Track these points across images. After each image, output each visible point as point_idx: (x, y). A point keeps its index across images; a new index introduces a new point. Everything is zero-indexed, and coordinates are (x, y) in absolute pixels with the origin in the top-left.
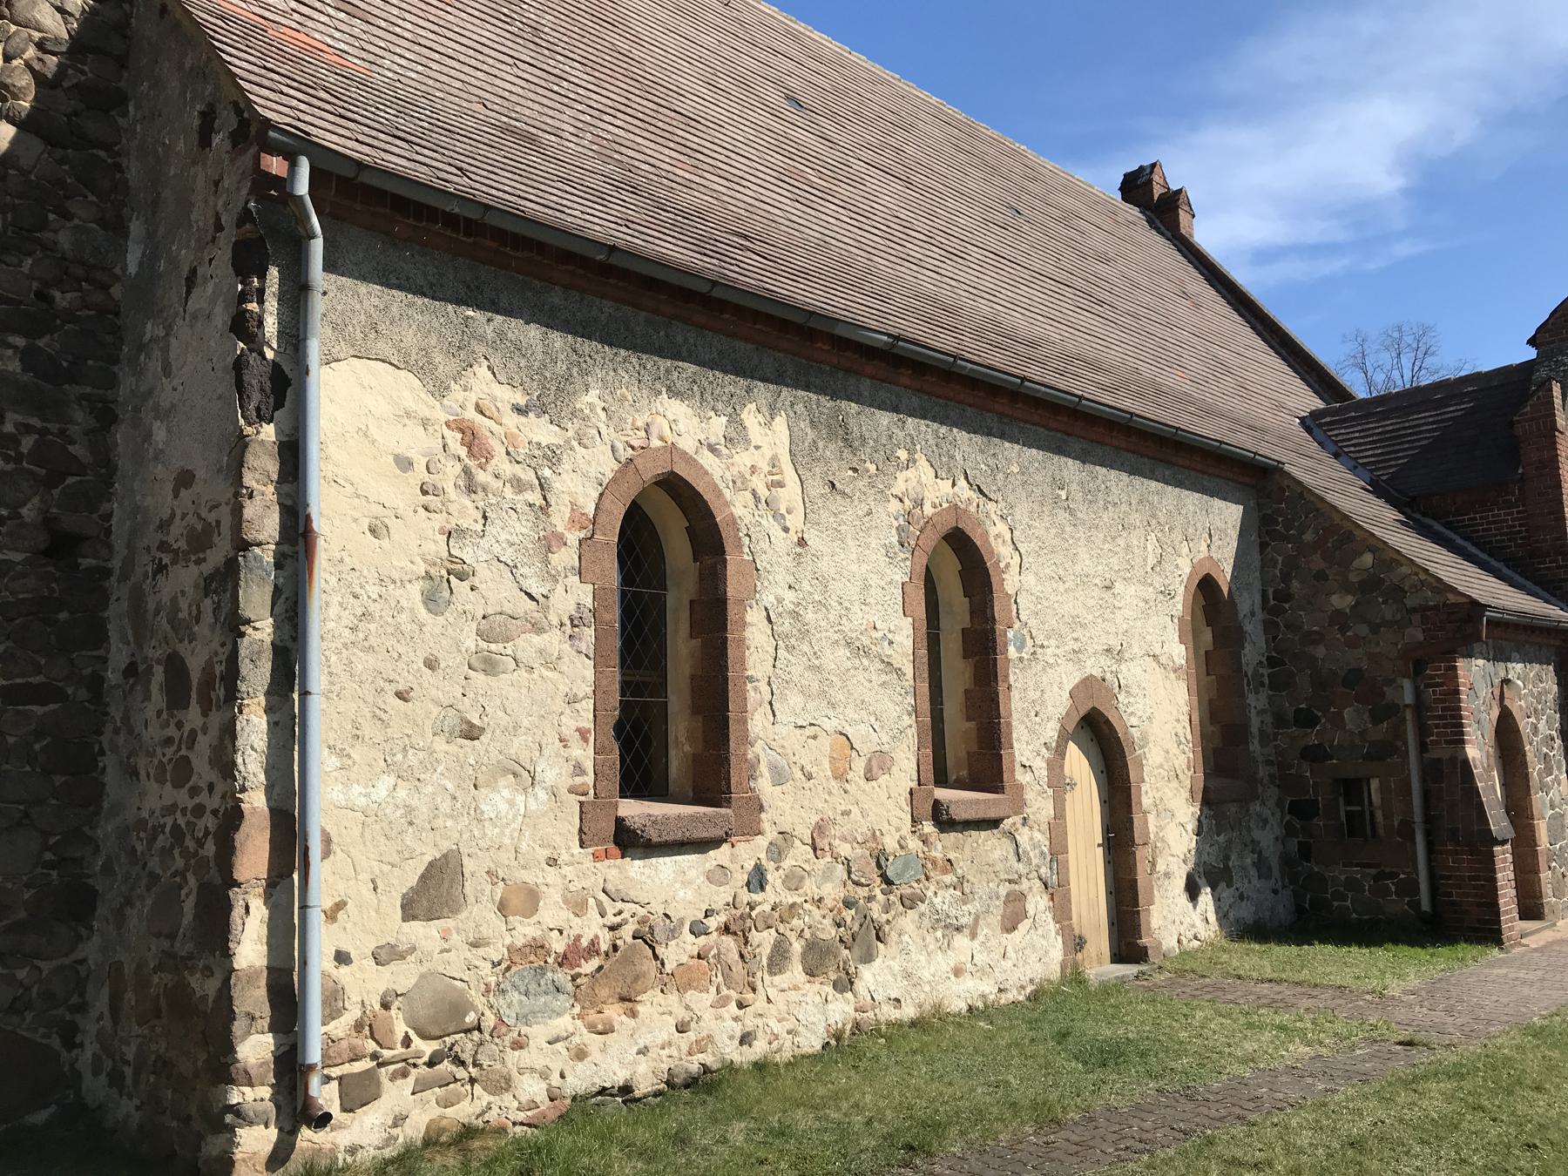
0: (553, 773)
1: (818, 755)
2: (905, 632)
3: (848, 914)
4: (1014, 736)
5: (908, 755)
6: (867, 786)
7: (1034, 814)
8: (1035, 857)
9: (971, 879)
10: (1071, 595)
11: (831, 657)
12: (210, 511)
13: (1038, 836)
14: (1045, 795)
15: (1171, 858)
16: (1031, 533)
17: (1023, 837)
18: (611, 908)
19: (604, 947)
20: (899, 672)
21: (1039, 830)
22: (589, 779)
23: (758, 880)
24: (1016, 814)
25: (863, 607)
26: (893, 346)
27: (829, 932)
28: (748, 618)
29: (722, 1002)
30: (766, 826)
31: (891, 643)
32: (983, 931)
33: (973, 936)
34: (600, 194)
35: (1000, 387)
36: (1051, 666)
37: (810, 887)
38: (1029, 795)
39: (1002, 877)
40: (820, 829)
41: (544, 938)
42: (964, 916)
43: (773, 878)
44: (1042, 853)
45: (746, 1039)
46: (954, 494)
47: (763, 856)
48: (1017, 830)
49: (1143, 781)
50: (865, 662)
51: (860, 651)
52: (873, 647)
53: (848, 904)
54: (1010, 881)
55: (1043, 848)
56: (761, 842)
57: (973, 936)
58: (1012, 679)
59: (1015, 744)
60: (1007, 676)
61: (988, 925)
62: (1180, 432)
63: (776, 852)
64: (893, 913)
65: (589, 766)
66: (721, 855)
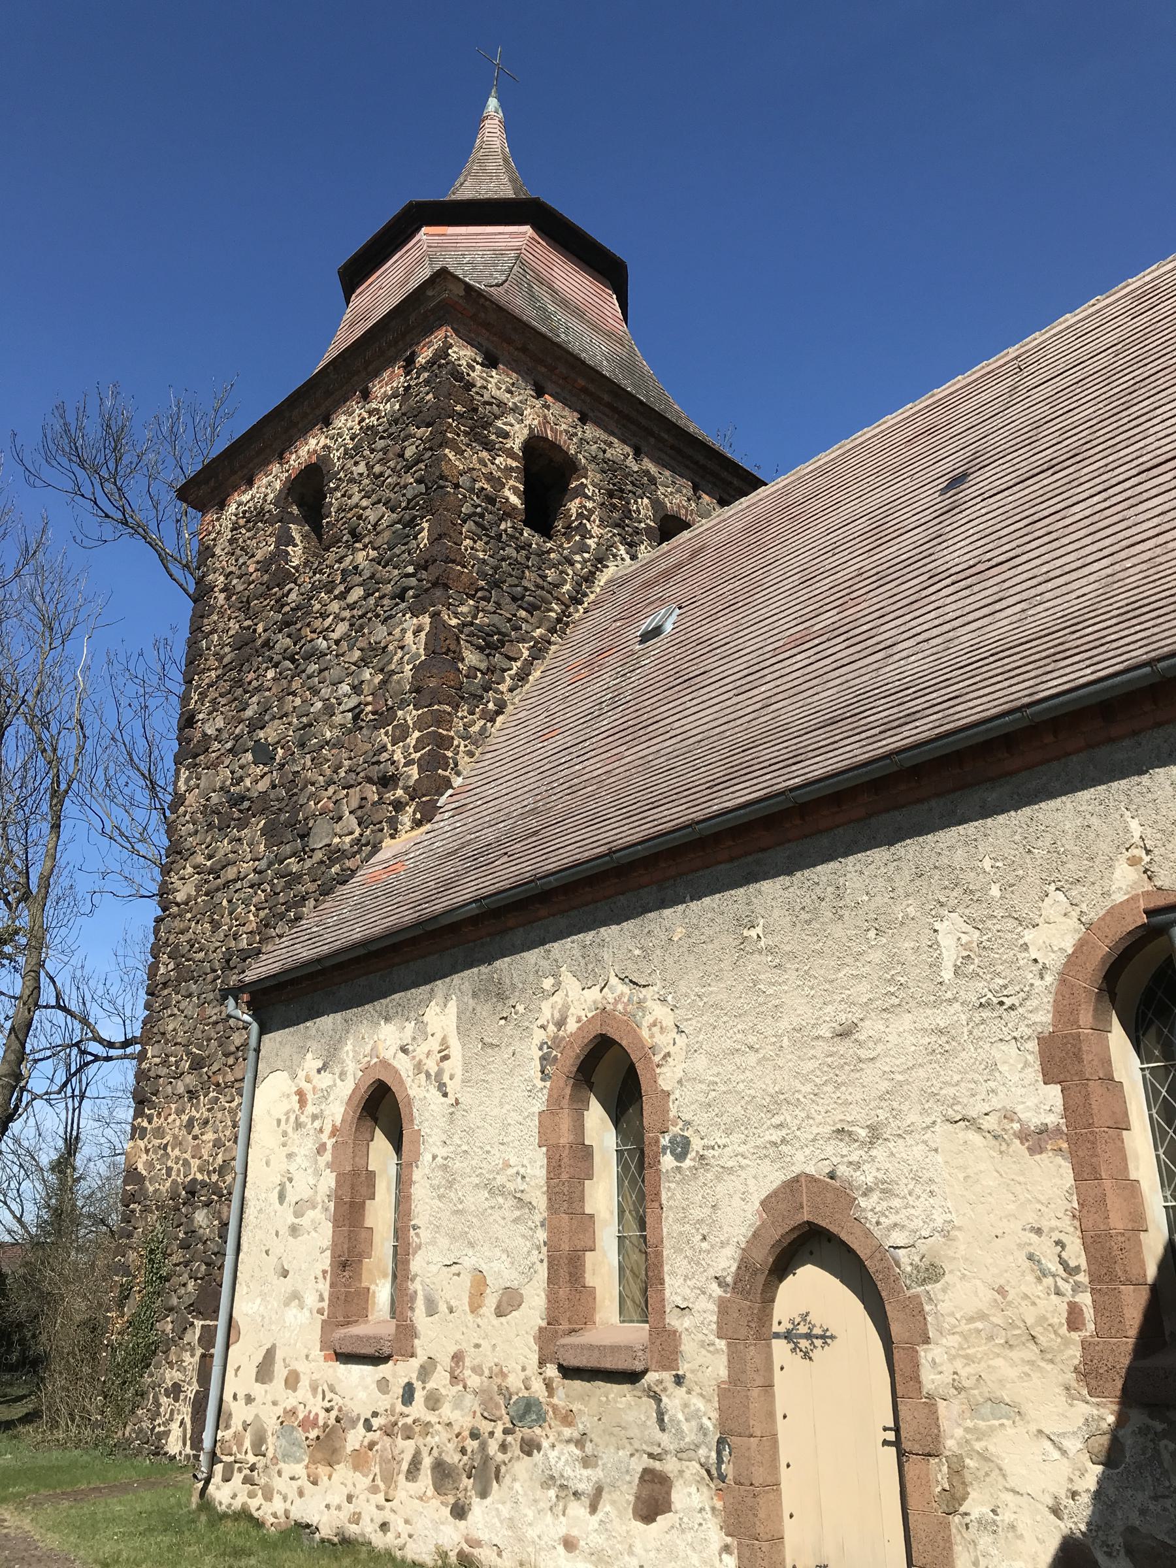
0: (311, 1300)
1: (456, 1292)
2: (539, 1163)
3: (472, 1445)
4: (666, 1268)
5: (538, 1291)
6: (496, 1321)
7: (693, 1371)
8: (691, 1431)
9: (596, 1439)
10: (769, 1065)
11: (472, 1200)
12: (1042, 978)
13: (698, 1403)
14: (711, 1348)
15: (1009, 1497)
16: (701, 1004)
17: (674, 1401)
18: (329, 1395)
19: (321, 1423)
20: (530, 1206)
21: (701, 1395)
22: (325, 1304)
23: (408, 1394)
24: (665, 1368)
25: (502, 1147)
26: (482, 906)
27: (452, 1457)
28: (415, 1178)
29: (374, 1490)
30: (419, 1351)
31: (523, 1177)
32: (605, 1507)
33: (593, 1509)
34: (1082, 649)
35: (857, 786)
36: (730, 1171)
37: (447, 1411)
38: (688, 1346)
39: (637, 1445)
40: (458, 1358)
41: (296, 1408)
42: (583, 1479)
43: (419, 1395)
44: (702, 1428)
45: (384, 1526)
46: (604, 997)
47: (414, 1375)
48: (665, 1390)
49: (927, 1340)
50: (501, 1200)
51: (495, 1191)
52: (508, 1185)
53: (474, 1435)
54: (651, 1456)
55: (705, 1420)
56: (415, 1363)
57: (593, 1509)
58: (664, 1196)
59: (667, 1278)
60: (658, 1194)
61: (613, 1503)
62: (1160, 665)
63: (425, 1372)
64: (509, 1455)
65: (326, 1296)
66: (384, 1370)
